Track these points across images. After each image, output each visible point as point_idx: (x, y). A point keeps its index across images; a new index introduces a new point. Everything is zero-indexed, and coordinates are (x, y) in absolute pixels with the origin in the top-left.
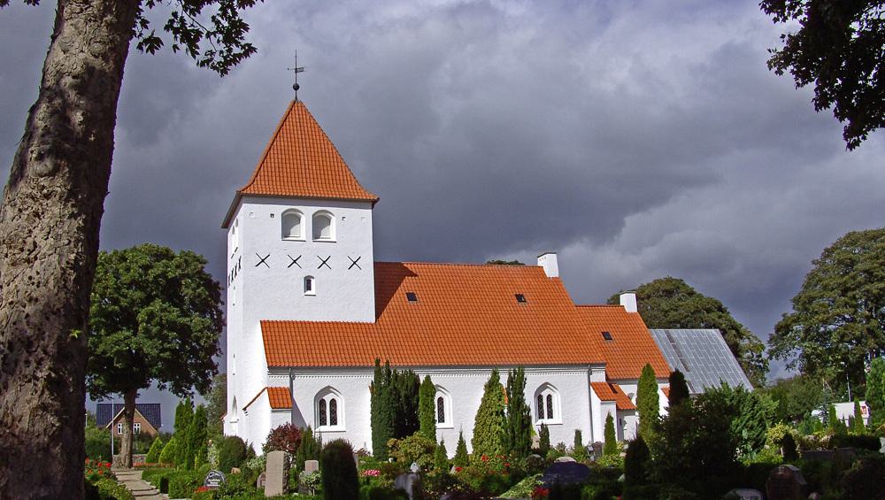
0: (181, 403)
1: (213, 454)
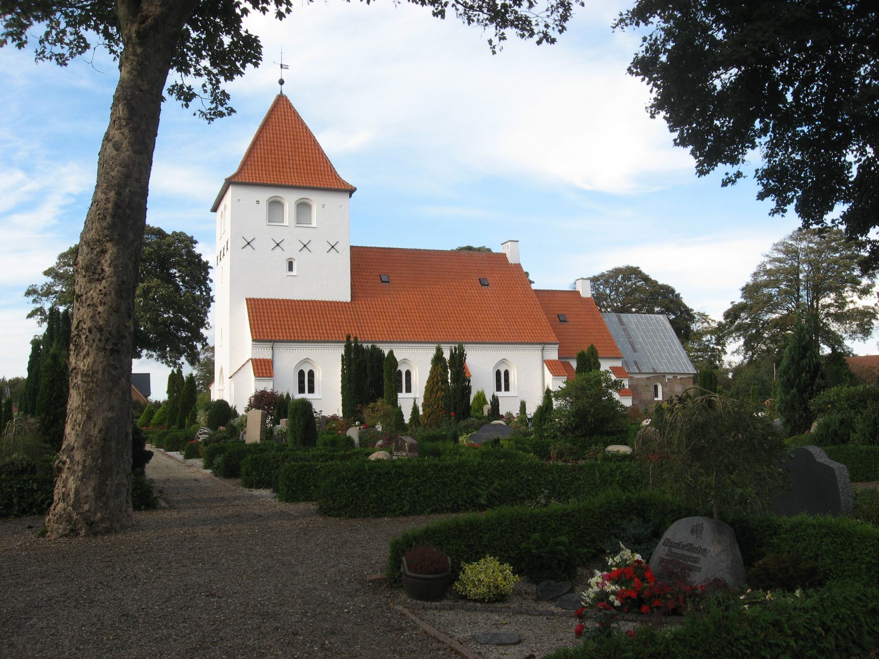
0: (173, 371)
1: (202, 417)
